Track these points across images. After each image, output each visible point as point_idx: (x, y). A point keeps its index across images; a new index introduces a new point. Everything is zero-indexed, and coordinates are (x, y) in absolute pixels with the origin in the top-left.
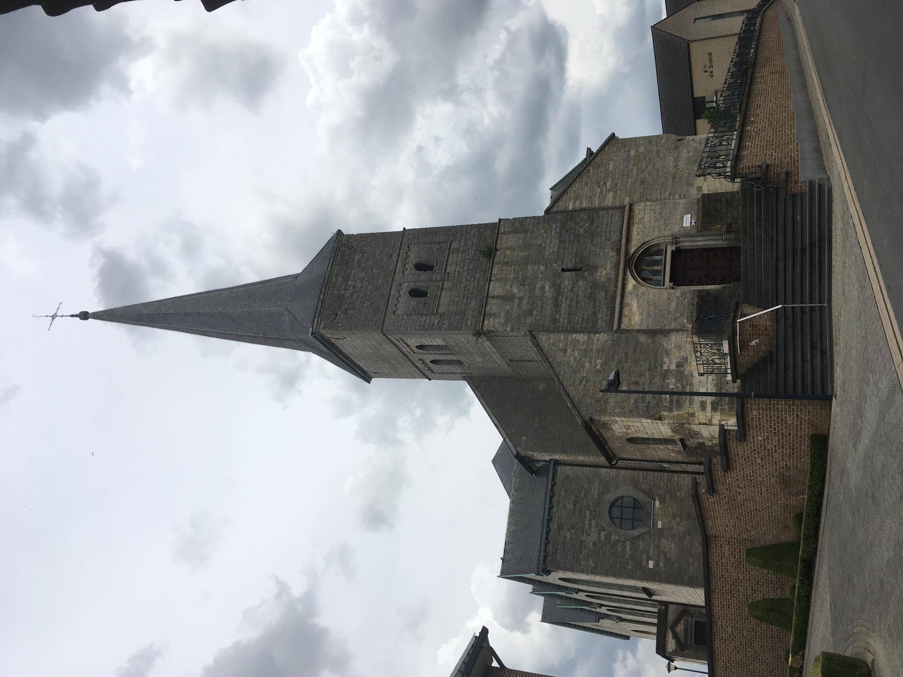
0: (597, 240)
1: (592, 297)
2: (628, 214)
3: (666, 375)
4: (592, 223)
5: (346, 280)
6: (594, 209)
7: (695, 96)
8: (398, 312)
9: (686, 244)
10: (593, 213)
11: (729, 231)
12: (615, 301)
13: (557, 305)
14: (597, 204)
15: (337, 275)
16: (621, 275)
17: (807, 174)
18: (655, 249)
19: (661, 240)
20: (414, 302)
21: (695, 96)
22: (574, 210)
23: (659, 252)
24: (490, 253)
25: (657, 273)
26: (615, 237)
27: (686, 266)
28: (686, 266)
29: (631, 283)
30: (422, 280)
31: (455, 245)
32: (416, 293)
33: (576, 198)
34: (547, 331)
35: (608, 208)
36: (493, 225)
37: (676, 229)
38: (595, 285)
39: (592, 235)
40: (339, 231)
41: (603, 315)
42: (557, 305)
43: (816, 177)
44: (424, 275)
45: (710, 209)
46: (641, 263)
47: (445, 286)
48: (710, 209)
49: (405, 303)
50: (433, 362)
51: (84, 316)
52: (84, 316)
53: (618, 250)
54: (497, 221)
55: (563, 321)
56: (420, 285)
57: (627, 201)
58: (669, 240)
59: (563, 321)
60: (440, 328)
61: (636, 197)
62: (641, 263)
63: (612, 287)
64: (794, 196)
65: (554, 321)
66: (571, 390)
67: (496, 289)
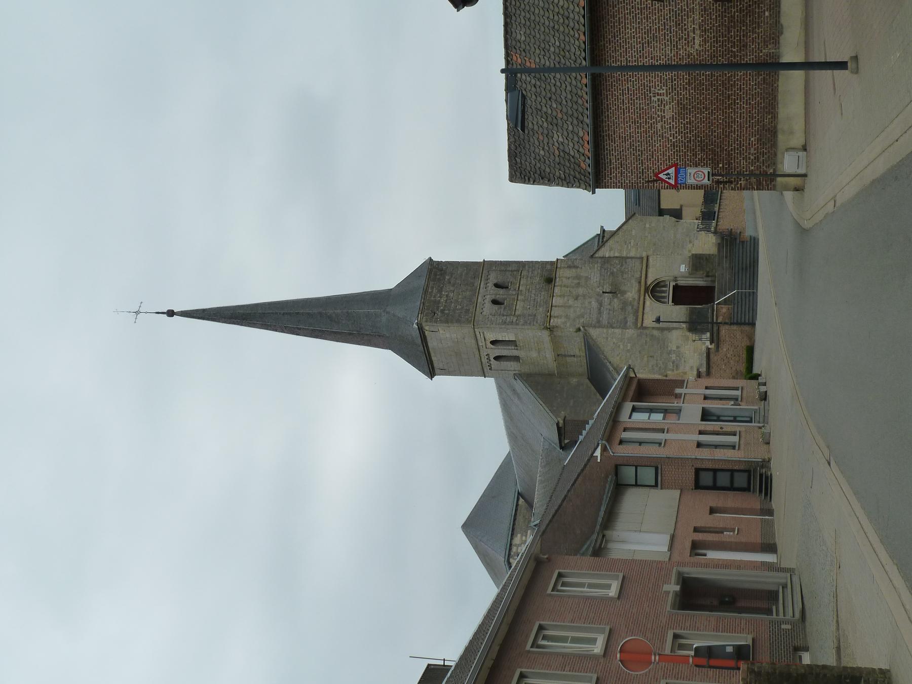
0: (625, 276)
1: (623, 309)
2: (645, 262)
3: (670, 353)
4: (622, 266)
5: (440, 291)
6: (623, 258)
7: (662, 207)
8: (484, 313)
9: (682, 282)
10: (623, 259)
11: (708, 276)
12: (639, 312)
13: (600, 312)
14: (624, 255)
15: (432, 288)
16: (642, 298)
17: (749, 233)
18: (662, 284)
19: (666, 278)
20: (496, 307)
21: (662, 207)
22: (610, 257)
23: (665, 286)
24: (550, 281)
25: (664, 297)
26: (637, 275)
27: (682, 295)
28: (682, 295)
29: (648, 303)
30: (500, 294)
31: (524, 273)
32: (495, 302)
33: (611, 250)
34: (595, 327)
35: (632, 258)
36: (552, 263)
37: (676, 273)
38: (624, 305)
39: (622, 272)
40: (430, 259)
41: (631, 319)
42: (600, 312)
43: (753, 234)
44: (501, 291)
45: (698, 262)
46: (655, 291)
47: (520, 297)
48: (698, 262)
49: (488, 308)
50: (497, 358)
51: (171, 313)
52: (171, 313)
53: (640, 283)
54: (555, 260)
55: (605, 318)
56: (498, 297)
57: (644, 255)
58: (672, 278)
59: (605, 318)
60: (517, 324)
61: (650, 253)
62: (655, 291)
63: (636, 303)
64: (743, 242)
65: (599, 322)
66: (611, 359)
67: (556, 301)
